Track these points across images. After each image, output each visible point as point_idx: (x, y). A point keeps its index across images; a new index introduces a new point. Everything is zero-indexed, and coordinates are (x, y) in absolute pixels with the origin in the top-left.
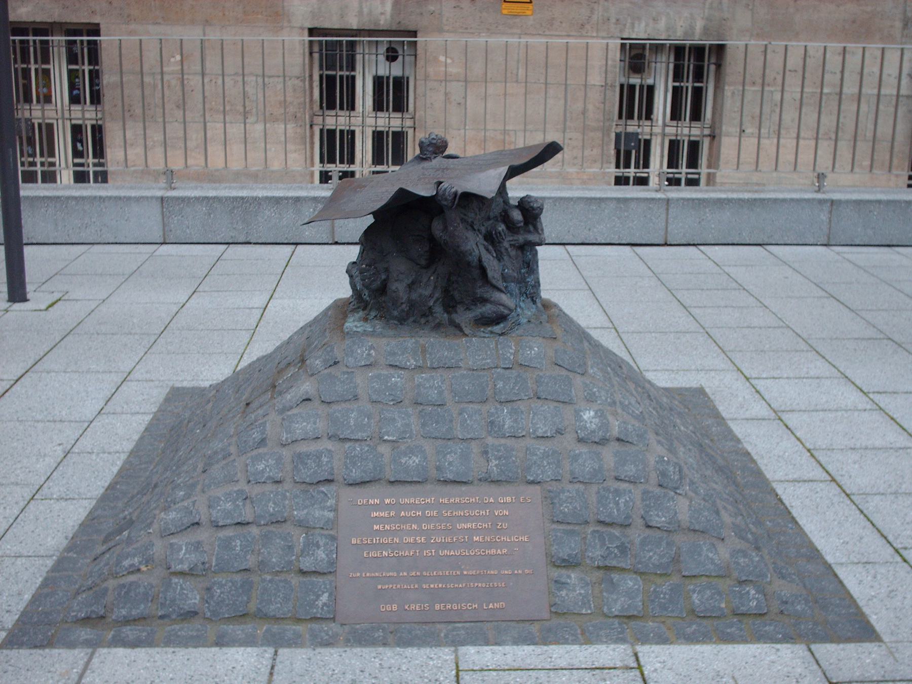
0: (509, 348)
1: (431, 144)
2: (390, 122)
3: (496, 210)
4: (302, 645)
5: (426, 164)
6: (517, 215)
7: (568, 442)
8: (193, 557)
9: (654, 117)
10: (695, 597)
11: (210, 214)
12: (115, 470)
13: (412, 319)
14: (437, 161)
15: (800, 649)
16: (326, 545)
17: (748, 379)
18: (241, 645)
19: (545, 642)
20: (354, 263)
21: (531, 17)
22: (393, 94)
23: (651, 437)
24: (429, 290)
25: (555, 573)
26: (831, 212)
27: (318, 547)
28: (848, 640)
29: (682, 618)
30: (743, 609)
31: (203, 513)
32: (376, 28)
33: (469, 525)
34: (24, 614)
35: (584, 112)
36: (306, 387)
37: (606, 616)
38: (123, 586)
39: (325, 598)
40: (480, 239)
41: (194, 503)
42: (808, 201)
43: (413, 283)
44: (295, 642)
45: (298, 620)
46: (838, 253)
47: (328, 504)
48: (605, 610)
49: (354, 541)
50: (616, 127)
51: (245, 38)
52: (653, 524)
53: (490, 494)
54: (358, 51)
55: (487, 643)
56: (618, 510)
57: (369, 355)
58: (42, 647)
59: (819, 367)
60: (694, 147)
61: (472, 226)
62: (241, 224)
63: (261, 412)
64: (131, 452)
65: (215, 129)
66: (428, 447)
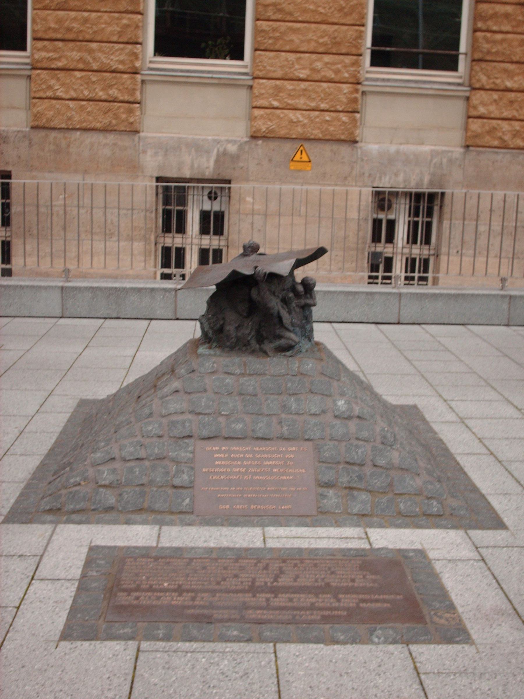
0: (295, 364)
1: (249, 247)
2: (211, 242)
3: (288, 284)
4: (175, 525)
5: (247, 258)
6: (300, 288)
7: (329, 417)
8: (111, 477)
9: (395, 241)
10: (402, 506)
11: (94, 299)
12: (53, 441)
13: (237, 348)
14: (253, 257)
15: (461, 532)
16: (188, 472)
17: (445, 401)
18: (140, 524)
19: (314, 526)
20: (203, 316)
21: (311, 172)
22: (213, 223)
23: (379, 419)
24: (248, 330)
25: (321, 490)
26: (510, 303)
27: (183, 473)
28: (489, 528)
29: (394, 517)
30: (429, 512)
31: (116, 453)
32: (203, 177)
33: (271, 463)
34: (12, 508)
35: (345, 237)
36: (176, 384)
37: (349, 514)
38: (71, 493)
39: (187, 501)
40: (278, 301)
41: (111, 448)
42: (494, 296)
43: (239, 326)
44: (171, 523)
45: (172, 513)
46: (515, 331)
47: (189, 449)
48: (349, 510)
49: (204, 470)
50: (370, 247)
51: (108, 183)
52: (378, 464)
53: (283, 446)
54: (189, 193)
55: (281, 526)
56: (358, 456)
57: (213, 366)
58: (26, 523)
59: (493, 395)
60: (426, 262)
61: (274, 294)
62: (115, 305)
63: (148, 399)
64: (61, 433)
65: (86, 246)
66: (247, 418)
